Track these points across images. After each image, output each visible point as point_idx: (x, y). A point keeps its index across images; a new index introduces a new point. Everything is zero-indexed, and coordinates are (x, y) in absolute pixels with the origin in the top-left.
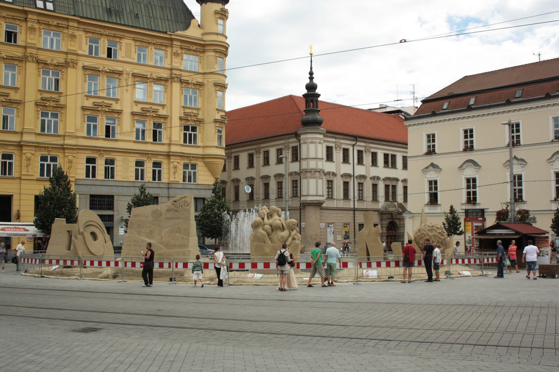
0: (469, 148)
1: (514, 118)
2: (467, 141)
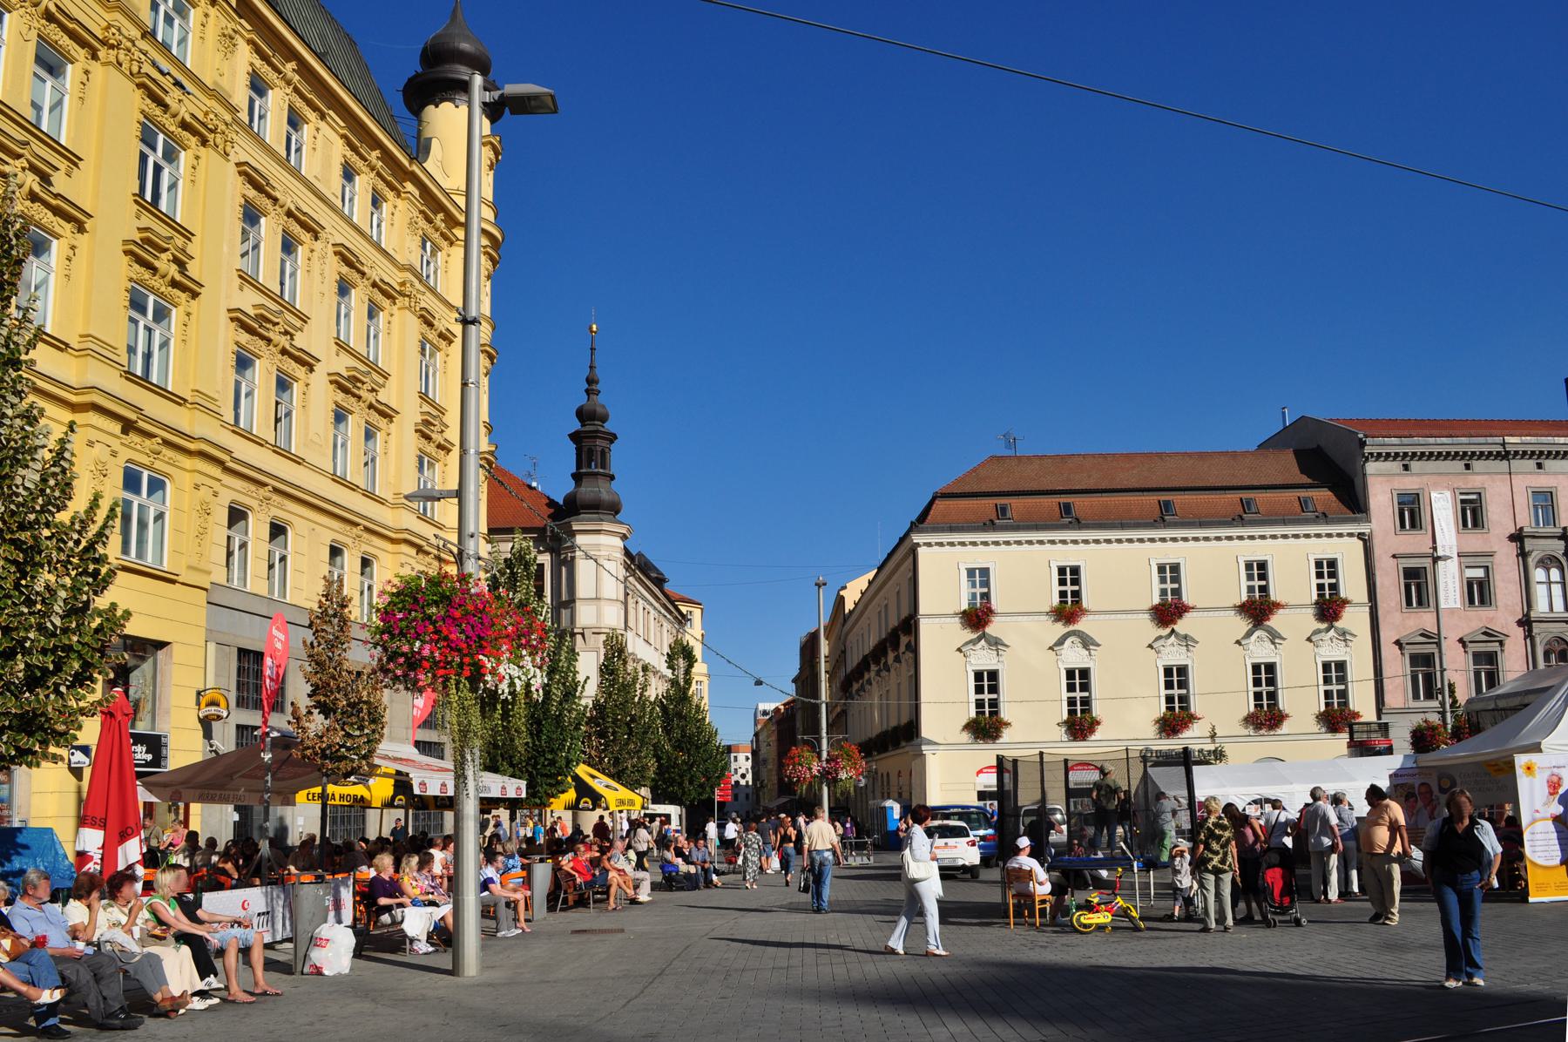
1: (1069, 555)
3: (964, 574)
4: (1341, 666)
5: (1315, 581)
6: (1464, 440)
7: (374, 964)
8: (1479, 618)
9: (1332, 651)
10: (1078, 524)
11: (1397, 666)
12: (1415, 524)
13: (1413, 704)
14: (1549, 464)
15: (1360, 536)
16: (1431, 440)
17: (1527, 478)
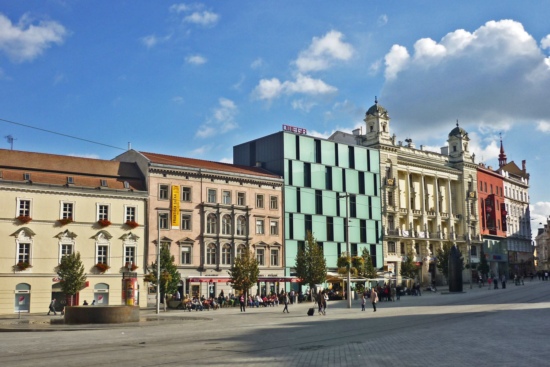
0: (24, 219)
2: (23, 211)
3: (126, 209)
4: (133, 249)
5: (126, 215)
6: (186, 168)
7: (283, 323)
9: (129, 243)
10: (30, 183)
11: (153, 250)
12: (166, 197)
14: (216, 181)
15: (145, 200)
16: (175, 167)
17: (207, 184)
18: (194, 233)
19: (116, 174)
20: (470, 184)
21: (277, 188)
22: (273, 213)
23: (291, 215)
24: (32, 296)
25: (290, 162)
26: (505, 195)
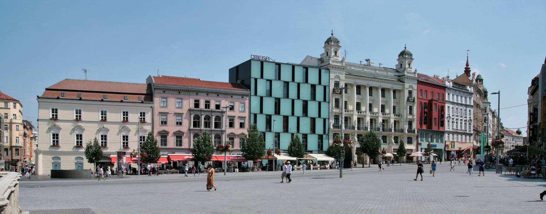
0: (104, 120)
8: (178, 128)
13: (175, 147)
18: (184, 128)
19: (145, 92)
20: (410, 93)
21: (245, 97)
22: (242, 115)
23: (255, 115)
24: (61, 164)
25: (256, 80)
26: (447, 99)
